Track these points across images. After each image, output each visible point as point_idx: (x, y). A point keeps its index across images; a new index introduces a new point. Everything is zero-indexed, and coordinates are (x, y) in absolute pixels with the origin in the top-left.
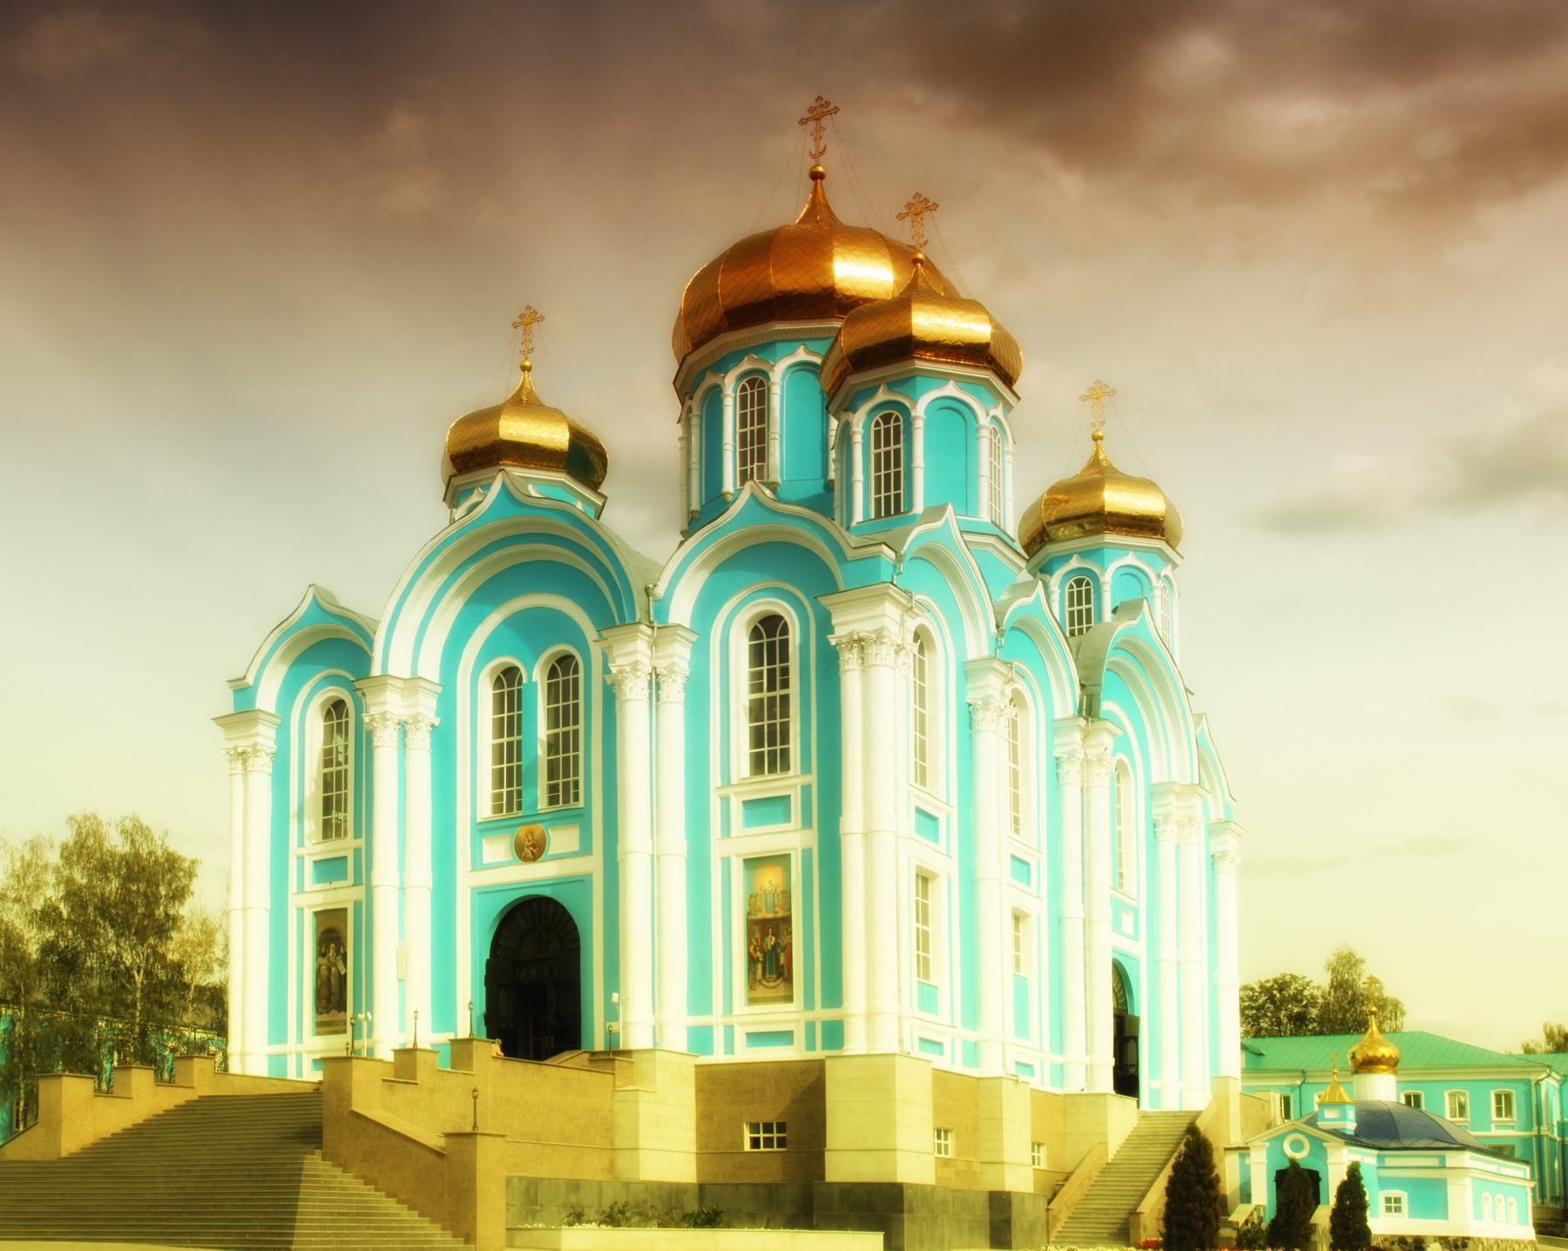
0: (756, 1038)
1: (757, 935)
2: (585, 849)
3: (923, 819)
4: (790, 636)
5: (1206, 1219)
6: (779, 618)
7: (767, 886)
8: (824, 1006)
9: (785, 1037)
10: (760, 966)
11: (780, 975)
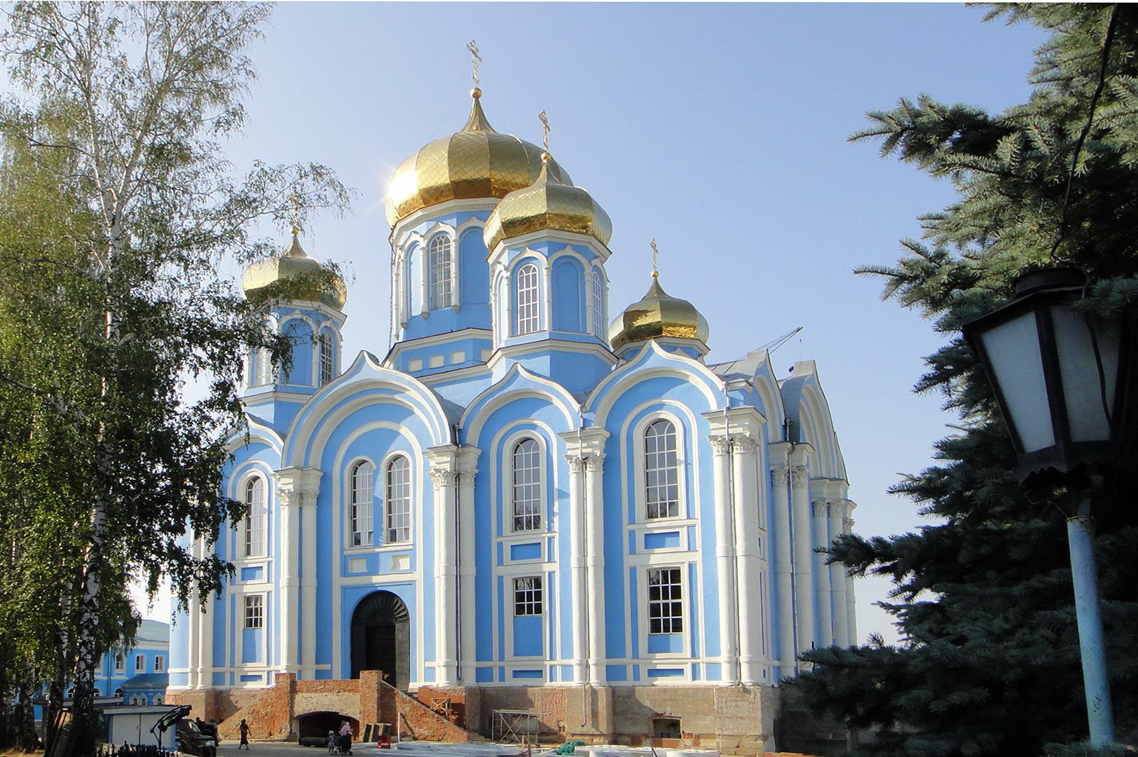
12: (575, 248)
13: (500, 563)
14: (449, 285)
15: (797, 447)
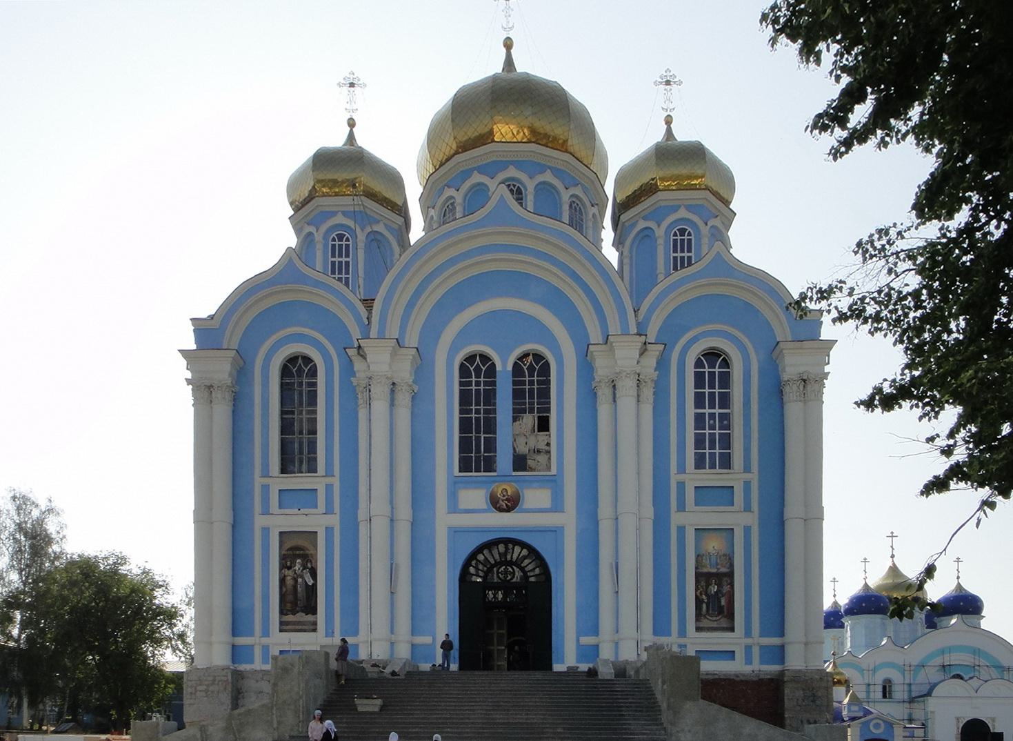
1: (703, 583)
6: (307, 360)
7: (711, 549)
9: (731, 655)
10: (704, 606)
11: (720, 611)
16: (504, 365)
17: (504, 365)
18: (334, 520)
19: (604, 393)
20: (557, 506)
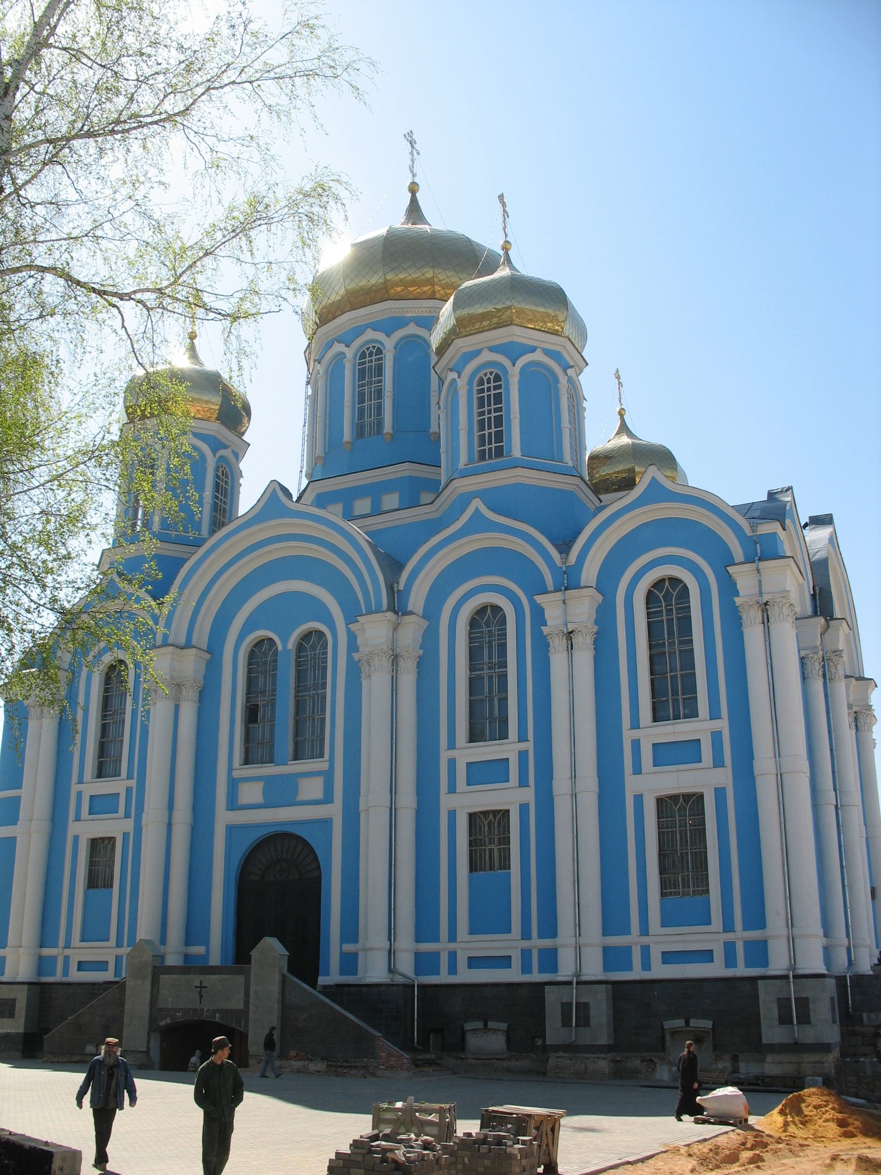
0: (474, 962)
2: (328, 799)
3: (748, 1093)
4: (24, 793)
5: (40, 653)
8: (540, 937)
12: (547, 352)
13: (452, 789)
14: (380, 408)
15: (832, 623)
16: (285, 644)
17: (285, 644)
18: (528, 795)
19: (558, 645)
20: (328, 799)
